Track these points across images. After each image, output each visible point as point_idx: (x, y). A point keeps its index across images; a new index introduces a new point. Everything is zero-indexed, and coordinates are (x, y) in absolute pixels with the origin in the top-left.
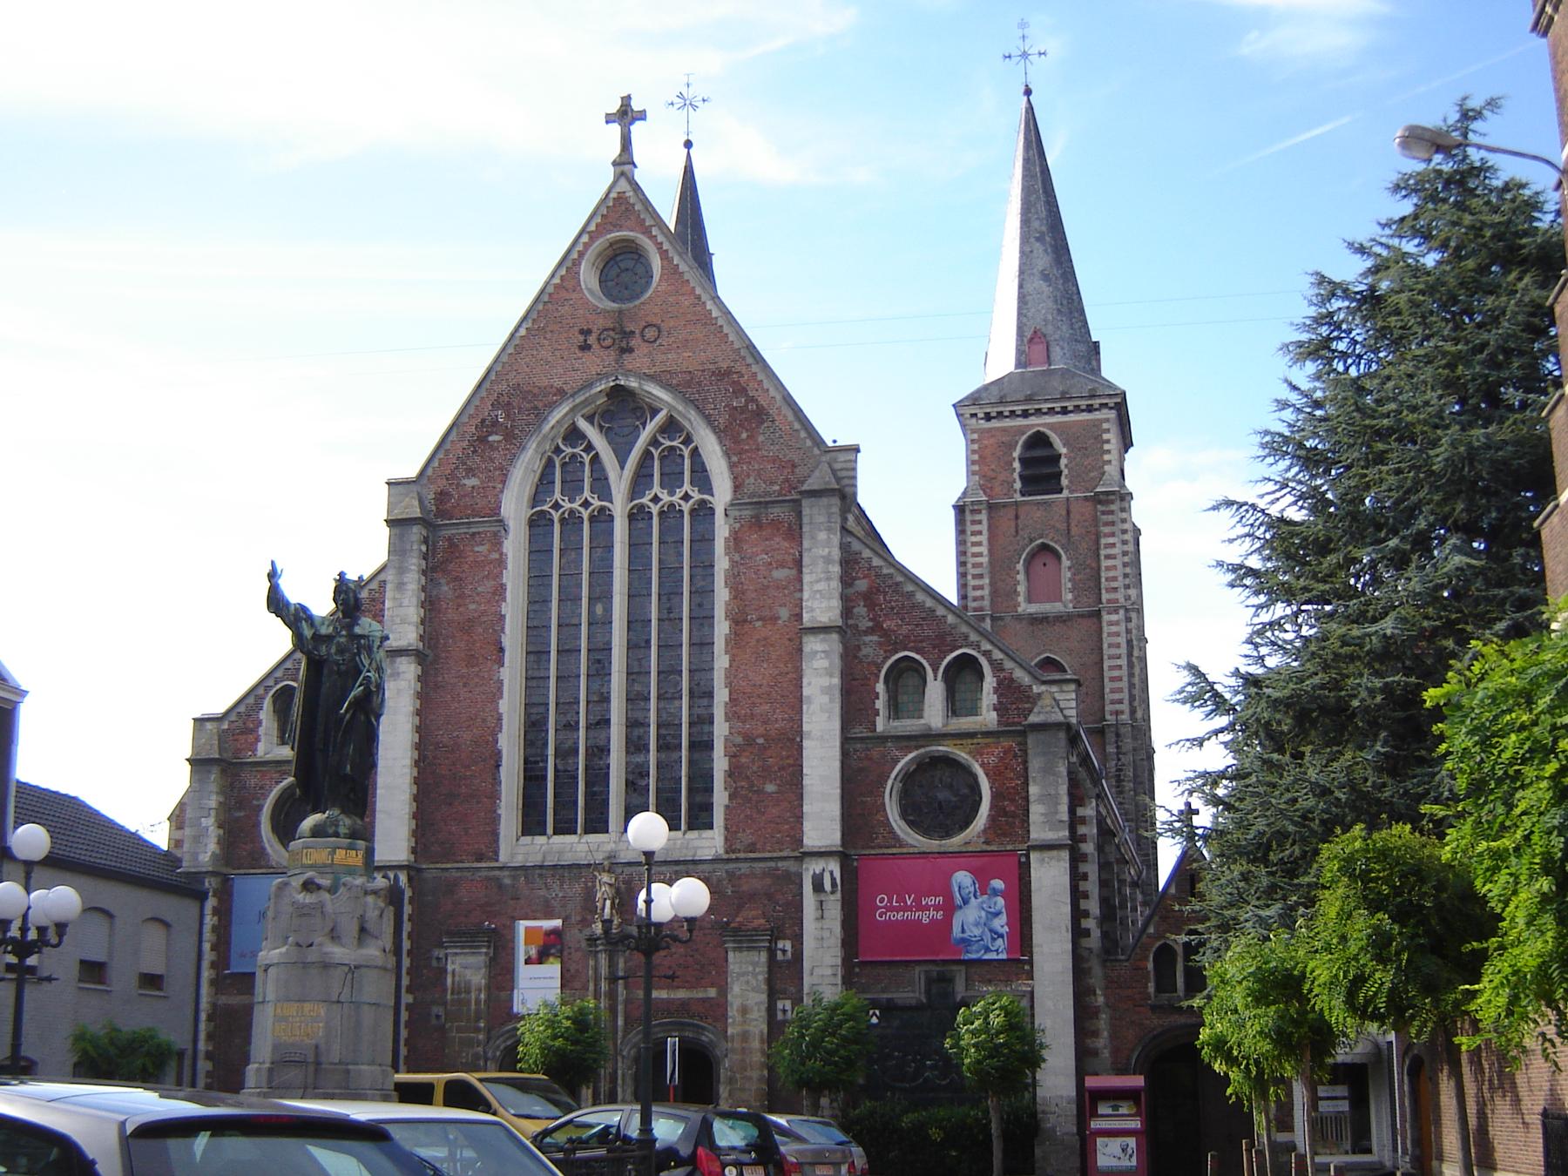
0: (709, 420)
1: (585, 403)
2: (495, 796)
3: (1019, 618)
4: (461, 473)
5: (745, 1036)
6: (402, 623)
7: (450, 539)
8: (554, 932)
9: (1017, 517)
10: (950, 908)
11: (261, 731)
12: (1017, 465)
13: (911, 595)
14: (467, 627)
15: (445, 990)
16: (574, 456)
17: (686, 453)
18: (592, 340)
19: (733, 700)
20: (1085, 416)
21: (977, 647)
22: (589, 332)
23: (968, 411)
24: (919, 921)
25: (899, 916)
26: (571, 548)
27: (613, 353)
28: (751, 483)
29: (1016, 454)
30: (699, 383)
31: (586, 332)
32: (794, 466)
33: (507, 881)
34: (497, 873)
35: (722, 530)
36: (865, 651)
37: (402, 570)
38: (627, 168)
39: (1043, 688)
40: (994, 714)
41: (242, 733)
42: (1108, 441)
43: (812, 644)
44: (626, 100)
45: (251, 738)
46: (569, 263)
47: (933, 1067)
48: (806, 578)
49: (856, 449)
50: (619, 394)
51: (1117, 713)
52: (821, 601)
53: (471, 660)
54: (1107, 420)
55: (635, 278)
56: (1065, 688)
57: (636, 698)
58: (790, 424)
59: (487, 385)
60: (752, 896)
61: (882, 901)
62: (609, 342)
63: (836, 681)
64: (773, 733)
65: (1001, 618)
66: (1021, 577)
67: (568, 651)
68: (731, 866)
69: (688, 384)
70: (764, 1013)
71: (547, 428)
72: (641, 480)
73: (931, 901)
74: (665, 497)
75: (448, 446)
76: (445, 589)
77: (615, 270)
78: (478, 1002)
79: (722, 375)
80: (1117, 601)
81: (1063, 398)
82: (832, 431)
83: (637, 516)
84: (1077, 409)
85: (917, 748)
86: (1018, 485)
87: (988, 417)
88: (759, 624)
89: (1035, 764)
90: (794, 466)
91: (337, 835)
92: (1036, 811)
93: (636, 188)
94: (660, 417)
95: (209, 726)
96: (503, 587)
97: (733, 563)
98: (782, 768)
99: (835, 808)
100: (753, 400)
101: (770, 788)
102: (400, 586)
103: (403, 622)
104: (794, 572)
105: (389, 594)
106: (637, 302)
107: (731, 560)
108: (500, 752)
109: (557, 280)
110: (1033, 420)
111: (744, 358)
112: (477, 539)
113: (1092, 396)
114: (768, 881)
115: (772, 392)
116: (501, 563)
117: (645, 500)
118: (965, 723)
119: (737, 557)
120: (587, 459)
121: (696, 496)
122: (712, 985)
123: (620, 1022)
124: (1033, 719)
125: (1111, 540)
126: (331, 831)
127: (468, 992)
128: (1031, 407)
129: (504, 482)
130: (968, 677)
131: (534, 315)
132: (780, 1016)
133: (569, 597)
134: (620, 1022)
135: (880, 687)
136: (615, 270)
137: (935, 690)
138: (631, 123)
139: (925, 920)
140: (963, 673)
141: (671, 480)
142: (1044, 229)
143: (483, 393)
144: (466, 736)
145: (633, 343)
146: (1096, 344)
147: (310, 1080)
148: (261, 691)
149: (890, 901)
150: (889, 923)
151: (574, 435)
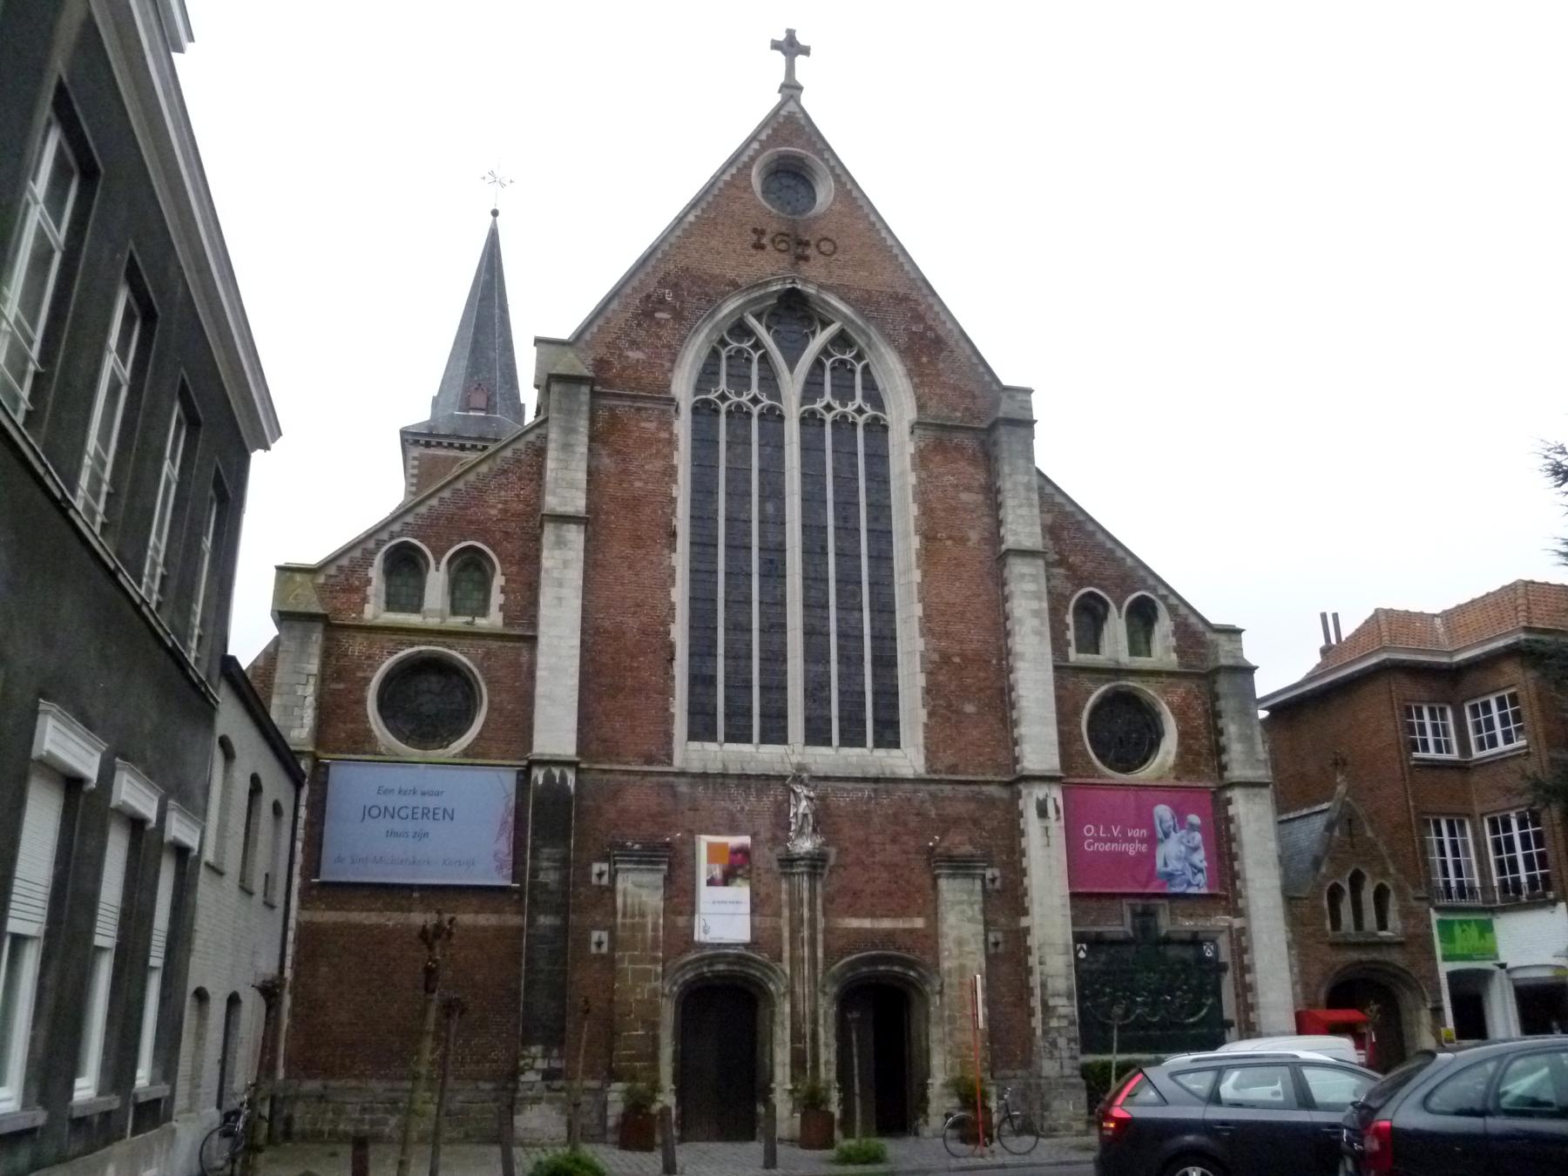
1: (762, 298)
4: (623, 343)
5: (962, 969)
7: (611, 409)
8: (742, 851)
10: (1152, 841)
11: (370, 590)
13: (1093, 534)
14: (633, 504)
15: (614, 913)
16: (740, 351)
17: (859, 368)
19: (927, 618)
21: (1154, 590)
24: (1126, 853)
25: (1107, 847)
26: (739, 442)
28: (933, 407)
31: (759, 232)
34: (671, 779)
40: (1174, 657)
41: (344, 591)
45: (356, 598)
46: (738, 164)
47: (1144, 1004)
49: (1029, 392)
53: (637, 541)
58: (969, 359)
60: (957, 822)
61: (1089, 831)
64: (969, 653)
67: (738, 547)
68: (933, 787)
70: (982, 946)
72: (812, 387)
73: (1136, 833)
75: (608, 313)
78: (655, 929)
82: (1008, 376)
83: (810, 421)
85: (1108, 681)
88: (949, 543)
90: (974, 397)
97: (921, 481)
98: (981, 690)
100: (931, 328)
101: (970, 708)
102: (567, 447)
107: (919, 477)
109: (727, 177)
114: (972, 806)
116: (671, 442)
118: (1141, 662)
119: (924, 475)
120: (756, 356)
121: (870, 412)
122: (919, 915)
123: (820, 954)
127: (643, 915)
129: (673, 361)
131: (704, 205)
133: (738, 494)
134: (820, 954)
139: (1132, 852)
141: (844, 392)
144: (632, 623)
145: (808, 252)
148: (371, 545)
149: (1097, 831)
150: (1097, 852)
151: (740, 329)
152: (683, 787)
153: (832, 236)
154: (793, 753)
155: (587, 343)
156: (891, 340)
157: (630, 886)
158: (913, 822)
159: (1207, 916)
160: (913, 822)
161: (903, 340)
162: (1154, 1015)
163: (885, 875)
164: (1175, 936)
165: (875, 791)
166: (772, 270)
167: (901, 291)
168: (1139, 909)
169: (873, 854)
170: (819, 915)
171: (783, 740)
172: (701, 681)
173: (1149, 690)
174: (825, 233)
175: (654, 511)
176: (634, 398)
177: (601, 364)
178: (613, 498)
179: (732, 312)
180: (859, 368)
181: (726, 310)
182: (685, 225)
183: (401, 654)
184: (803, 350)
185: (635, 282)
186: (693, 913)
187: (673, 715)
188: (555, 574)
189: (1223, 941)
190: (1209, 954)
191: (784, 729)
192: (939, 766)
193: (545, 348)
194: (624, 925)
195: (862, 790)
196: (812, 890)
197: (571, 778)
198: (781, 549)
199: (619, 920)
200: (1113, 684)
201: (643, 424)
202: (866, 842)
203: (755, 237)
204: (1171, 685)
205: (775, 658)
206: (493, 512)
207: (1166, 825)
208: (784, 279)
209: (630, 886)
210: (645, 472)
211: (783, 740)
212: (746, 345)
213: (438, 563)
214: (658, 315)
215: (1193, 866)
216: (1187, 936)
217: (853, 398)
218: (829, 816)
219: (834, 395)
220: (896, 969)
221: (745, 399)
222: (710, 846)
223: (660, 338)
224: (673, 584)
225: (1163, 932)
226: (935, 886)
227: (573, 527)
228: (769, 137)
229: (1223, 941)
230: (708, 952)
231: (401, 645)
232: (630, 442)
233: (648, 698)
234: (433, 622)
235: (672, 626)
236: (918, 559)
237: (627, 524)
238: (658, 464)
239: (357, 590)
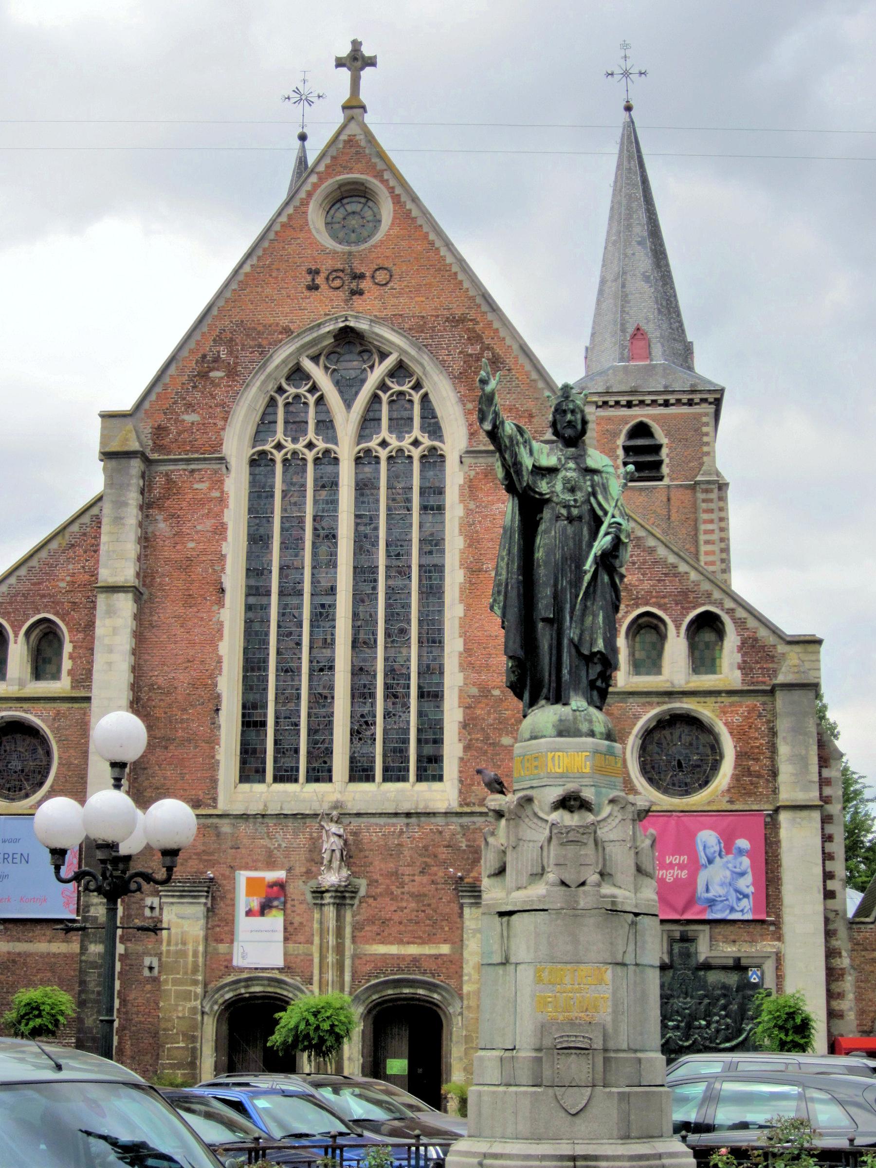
4: (179, 408)
6: (118, 562)
7: (167, 475)
8: (281, 886)
10: (694, 867)
14: (187, 565)
16: (297, 397)
18: (320, 280)
19: (468, 651)
20: (685, 410)
21: (720, 604)
22: (317, 272)
26: (294, 490)
30: (433, 329)
32: (531, 416)
37: (120, 504)
40: (738, 674)
47: (677, 1028)
53: (189, 600)
54: (706, 415)
57: (361, 643)
58: (528, 374)
59: (209, 320)
62: (337, 283)
68: (465, 820)
72: (369, 422)
73: (676, 859)
75: (166, 379)
76: (162, 527)
77: (340, 214)
79: (456, 321)
83: (364, 459)
89: (783, 725)
91: (592, 734)
92: (786, 771)
94: (390, 362)
97: (469, 512)
102: (118, 520)
105: (105, 528)
106: (367, 245)
108: (219, 696)
109: (283, 219)
111: (479, 306)
112: (197, 475)
113: (693, 392)
115: (508, 341)
116: (222, 501)
117: (373, 444)
118: (706, 681)
120: (311, 399)
121: (427, 442)
122: (445, 941)
123: (347, 977)
124: (781, 679)
125: (710, 527)
126: (584, 727)
127: (184, 943)
128: (635, 399)
129: (226, 419)
130: (708, 636)
136: (340, 214)
137: (676, 646)
138: (362, 69)
140: (707, 625)
141: (401, 424)
142: (646, 234)
143: (205, 328)
144: (183, 678)
147: (599, 1076)
151: (297, 374)
152: (226, 827)
154: (339, 790)
155: (146, 411)
156: (443, 365)
157: (174, 919)
158: (443, 853)
159: (753, 941)
160: (443, 853)
161: (458, 366)
162: (687, 1040)
163: (413, 905)
164: (714, 962)
165: (407, 825)
166: (327, 312)
167: (458, 313)
168: (677, 935)
169: (402, 885)
170: (348, 942)
172: (251, 723)
173: (705, 711)
174: (380, 262)
175: (205, 570)
176: (188, 461)
177: (160, 431)
178: (167, 561)
179: (284, 362)
180: (416, 397)
181: (278, 359)
182: (241, 277)
185: (192, 344)
186: (232, 942)
187: (218, 762)
188: (107, 641)
189: (769, 967)
190: (754, 979)
192: (472, 799)
194: (168, 951)
195: (394, 825)
196: (339, 918)
199: (164, 948)
200: (665, 707)
201: (196, 486)
202: (395, 874)
204: (732, 704)
205: (322, 699)
206: (63, 585)
207: (710, 851)
208: (336, 319)
209: (174, 919)
210: (197, 532)
212: (302, 390)
213: (16, 636)
214: (212, 374)
215: (737, 891)
216: (730, 962)
217: (305, 432)
218: (361, 851)
220: (421, 991)
221: (300, 446)
222: (249, 879)
224: (221, 638)
225: (702, 958)
226: (461, 915)
227: (121, 596)
228: (327, 167)
229: (769, 967)
230: (245, 975)
232: (184, 504)
233: (196, 747)
235: (219, 679)
236: (462, 591)
237: (180, 584)
238: (209, 524)
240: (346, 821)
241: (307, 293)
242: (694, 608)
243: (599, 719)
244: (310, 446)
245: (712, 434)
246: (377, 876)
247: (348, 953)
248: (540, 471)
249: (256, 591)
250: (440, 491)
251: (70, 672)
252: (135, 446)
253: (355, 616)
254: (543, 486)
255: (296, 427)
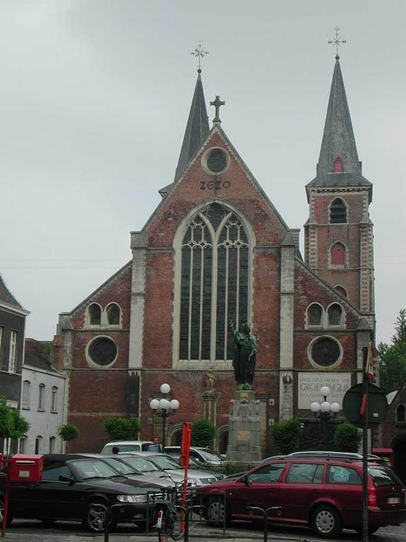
0: (247, 217)
2: (171, 345)
3: (328, 271)
7: (154, 255)
9: (328, 231)
12: (329, 211)
14: (161, 286)
16: (198, 226)
17: (239, 228)
20: (357, 193)
21: (340, 302)
22: (204, 183)
23: (310, 189)
26: (197, 260)
27: (213, 191)
29: (329, 206)
33: (175, 376)
35: (252, 257)
36: (301, 301)
38: (218, 123)
39: (362, 317)
42: (365, 203)
43: (284, 299)
44: (217, 97)
48: (282, 276)
50: (215, 205)
51: (365, 309)
52: (287, 284)
55: (207, 152)
56: (370, 317)
62: (211, 187)
63: (292, 312)
65: (321, 270)
66: (329, 255)
69: (240, 204)
71: (189, 216)
72: (222, 237)
74: (231, 244)
80: (366, 266)
81: (348, 186)
84: (354, 190)
86: (329, 219)
87: (319, 192)
93: (222, 132)
95: (65, 317)
96: (173, 273)
97: (256, 269)
99: (291, 355)
100: (263, 211)
101: (267, 347)
102: (137, 271)
103: (138, 284)
104: (277, 273)
105: (133, 274)
110: (336, 194)
113: (360, 186)
116: (173, 264)
120: (203, 228)
132: (270, 424)
135: (306, 314)
137: (325, 315)
140: (336, 309)
141: (233, 237)
146: (361, 163)
151: (198, 219)
153: (228, 180)
167: (254, 198)
171: (209, 358)
172: (183, 339)
177: (151, 239)
183: (94, 338)
184: (220, 222)
191: (209, 356)
193: (134, 236)
196: (212, 405)
197: (139, 373)
198: (210, 295)
203: (201, 185)
211: (209, 358)
214: (169, 219)
217: (201, 239)
219: (194, 240)
223: (169, 227)
231: (94, 335)
234: (103, 328)
239: (81, 319)
240: (214, 373)
241: (201, 191)
242: (330, 303)
243: (250, 386)
244: (203, 244)
245: (367, 203)
246: (224, 391)
247: (215, 417)
248: (241, 340)
249: (184, 294)
250: (247, 261)
251: (122, 322)
252: (144, 245)
253: (218, 303)
254: (242, 343)
255: (198, 238)
